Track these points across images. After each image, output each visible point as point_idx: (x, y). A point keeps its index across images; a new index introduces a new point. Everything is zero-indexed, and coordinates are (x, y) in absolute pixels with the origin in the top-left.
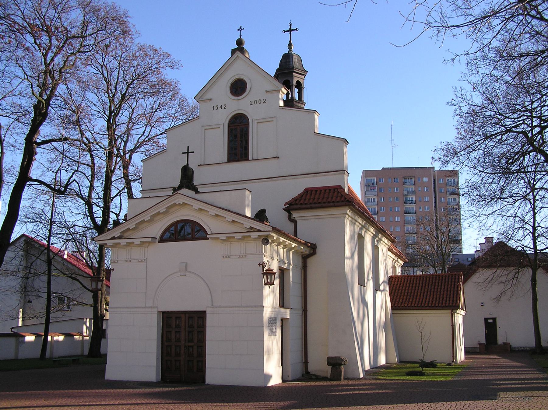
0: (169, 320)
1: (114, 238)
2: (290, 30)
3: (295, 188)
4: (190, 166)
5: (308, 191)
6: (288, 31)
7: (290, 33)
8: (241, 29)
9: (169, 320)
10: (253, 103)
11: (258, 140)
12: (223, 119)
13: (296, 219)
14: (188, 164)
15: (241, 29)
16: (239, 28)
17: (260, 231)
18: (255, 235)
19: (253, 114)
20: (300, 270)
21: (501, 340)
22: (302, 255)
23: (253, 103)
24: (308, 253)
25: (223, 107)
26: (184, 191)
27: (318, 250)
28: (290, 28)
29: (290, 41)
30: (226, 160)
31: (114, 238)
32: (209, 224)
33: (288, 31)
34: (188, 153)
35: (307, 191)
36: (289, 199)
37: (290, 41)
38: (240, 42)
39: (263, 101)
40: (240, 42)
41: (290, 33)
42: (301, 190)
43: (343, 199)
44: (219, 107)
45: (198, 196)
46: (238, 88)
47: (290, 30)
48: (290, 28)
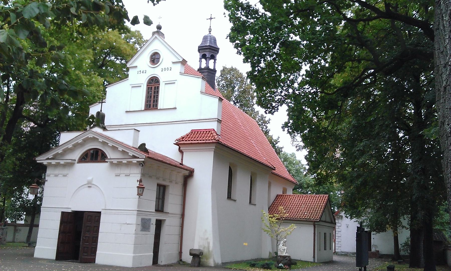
1: (48, 159)
2: (211, 19)
3: (184, 130)
11: (165, 97)
12: (143, 80)
14: (101, 111)
17: (138, 158)
18: (135, 161)
25: (144, 72)
27: (196, 174)
30: (143, 109)
31: (48, 159)
32: (110, 154)
35: (192, 131)
36: (179, 137)
39: (169, 69)
42: (188, 131)
44: (142, 71)
47: (211, 19)
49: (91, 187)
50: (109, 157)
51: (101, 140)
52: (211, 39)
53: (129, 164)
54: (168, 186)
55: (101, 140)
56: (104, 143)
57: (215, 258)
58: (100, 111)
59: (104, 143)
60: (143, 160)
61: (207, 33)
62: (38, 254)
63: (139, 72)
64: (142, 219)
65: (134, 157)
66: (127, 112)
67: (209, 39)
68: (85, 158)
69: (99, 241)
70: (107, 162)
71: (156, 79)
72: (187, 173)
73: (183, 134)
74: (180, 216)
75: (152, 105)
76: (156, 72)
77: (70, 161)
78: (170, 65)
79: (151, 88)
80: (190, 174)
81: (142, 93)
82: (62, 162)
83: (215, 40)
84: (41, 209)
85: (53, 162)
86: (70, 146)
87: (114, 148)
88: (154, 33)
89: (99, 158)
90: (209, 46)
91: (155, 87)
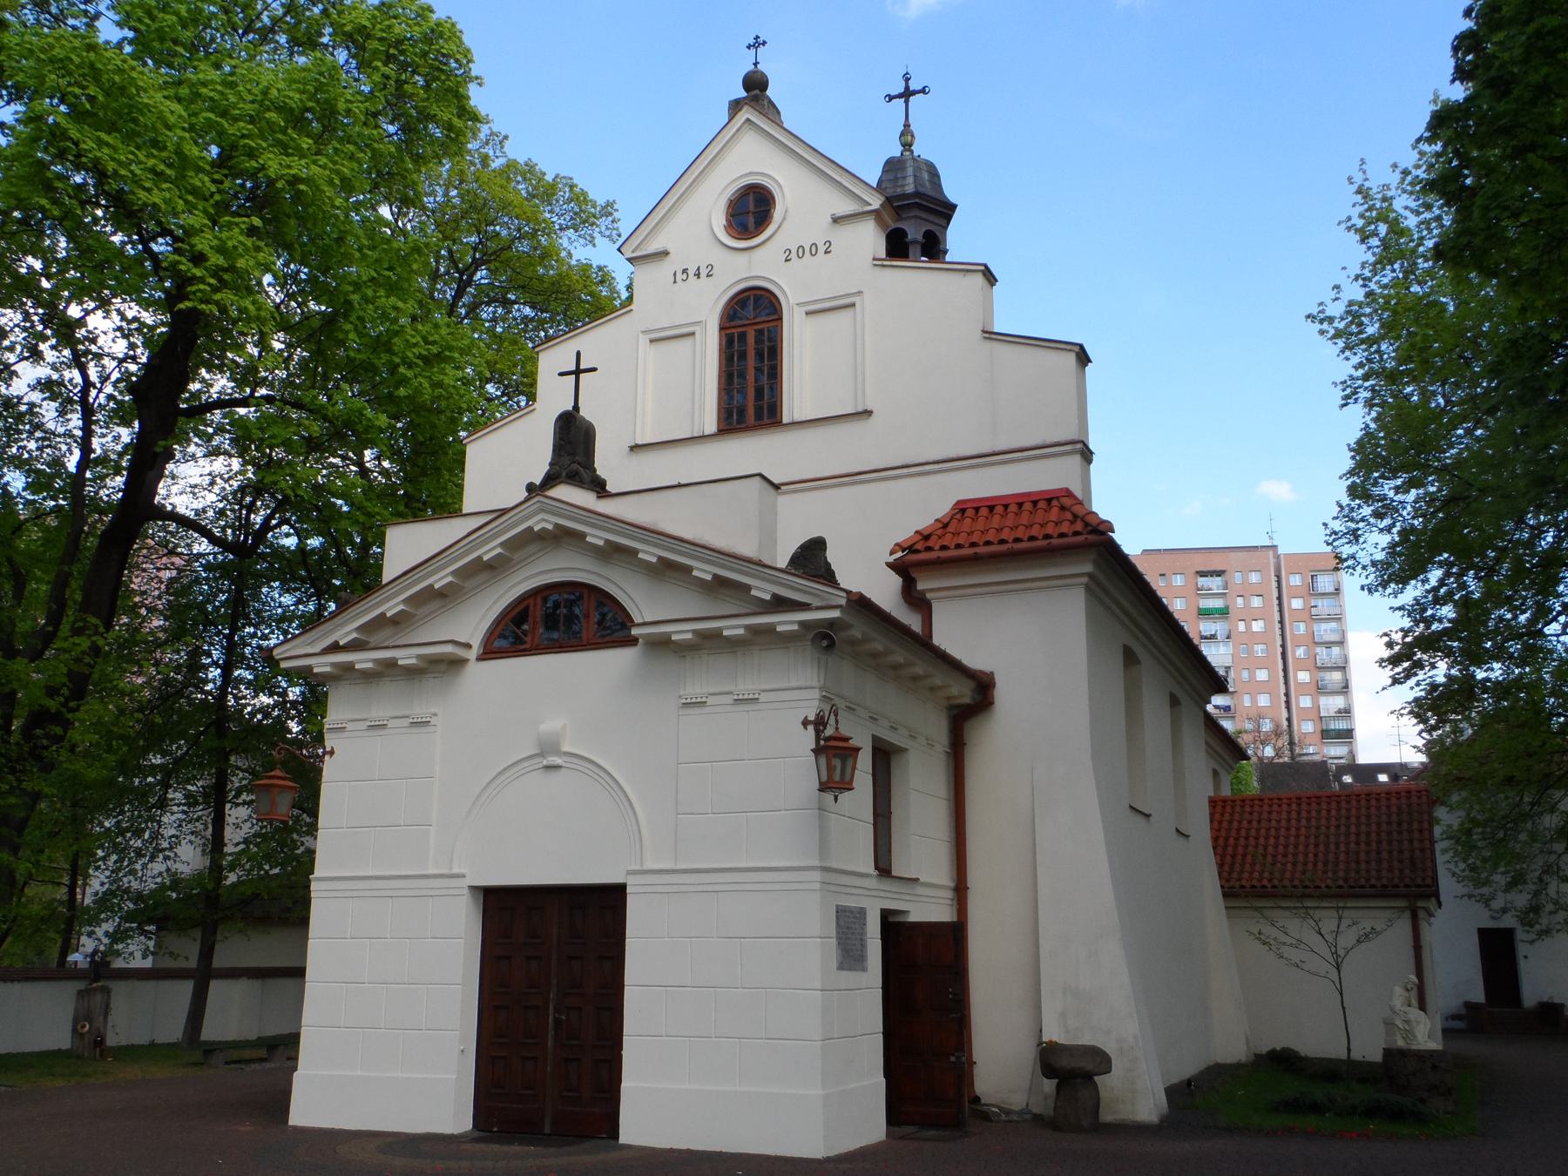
0: (506, 910)
1: (335, 648)
2: (907, 94)
3: (922, 506)
4: (584, 412)
5: (963, 511)
6: (899, 96)
7: (907, 102)
8: (757, 43)
9: (506, 910)
10: (794, 255)
11: (809, 370)
12: (704, 308)
13: (928, 596)
14: (576, 407)
15: (757, 43)
16: (752, 41)
17: (804, 607)
18: (786, 622)
19: (794, 288)
20: (943, 757)
21: (1531, 995)
22: (951, 708)
23: (794, 255)
24: (967, 700)
25: (704, 272)
26: (564, 492)
27: (1001, 693)
28: (907, 87)
29: (907, 126)
30: (711, 426)
31: (335, 648)
32: (646, 605)
33: (899, 96)
34: (577, 372)
35: (962, 509)
36: (905, 533)
37: (907, 126)
38: (755, 85)
39: (822, 249)
40: (755, 85)
41: (907, 102)
42: (943, 509)
43: (1079, 526)
44: (691, 272)
45: (605, 506)
46: (751, 210)
47: (907, 94)
48: (907, 87)
49: (558, 767)
50: (637, 620)
51: (596, 538)
52: (917, 169)
53: (762, 637)
54: (901, 750)
55: (596, 538)
56: (614, 553)
57: (1137, 1091)
58: (896, 150)
59: (614, 553)
60: (835, 614)
61: (896, 150)
62: (321, 1098)
63: (680, 276)
64: (841, 912)
65: (780, 604)
66: (635, 448)
67: (910, 171)
68: (521, 632)
69: (880, 1037)
70: (633, 641)
71: (757, 299)
72: (962, 692)
73: (924, 519)
74: (949, 894)
75: (751, 411)
76: (763, 263)
77: (449, 649)
78: (818, 230)
79: (743, 336)
80: (973, 699)
81: (705, 357)
82: (406, 657)
83: (934, 174)
84: (314, 886)
85: (363, 660)
86: (440, 579)
87: (668, 571)
88: (736, 106)
89: (589, 628)
90: (917, 194)
91: (760, 332)
